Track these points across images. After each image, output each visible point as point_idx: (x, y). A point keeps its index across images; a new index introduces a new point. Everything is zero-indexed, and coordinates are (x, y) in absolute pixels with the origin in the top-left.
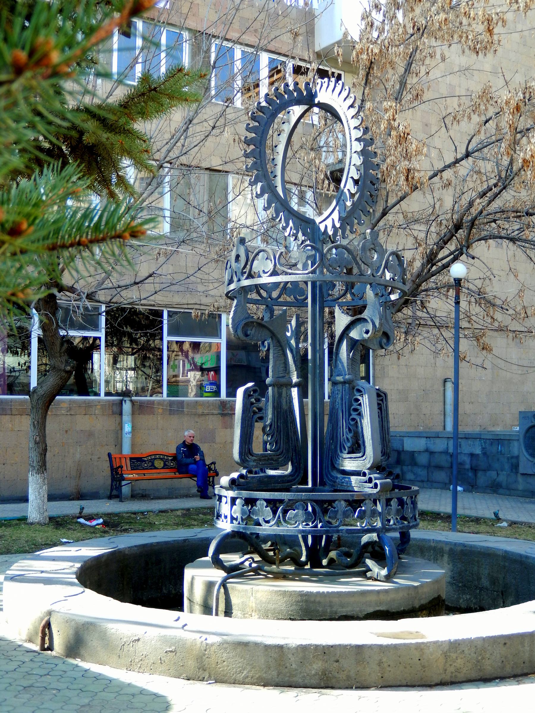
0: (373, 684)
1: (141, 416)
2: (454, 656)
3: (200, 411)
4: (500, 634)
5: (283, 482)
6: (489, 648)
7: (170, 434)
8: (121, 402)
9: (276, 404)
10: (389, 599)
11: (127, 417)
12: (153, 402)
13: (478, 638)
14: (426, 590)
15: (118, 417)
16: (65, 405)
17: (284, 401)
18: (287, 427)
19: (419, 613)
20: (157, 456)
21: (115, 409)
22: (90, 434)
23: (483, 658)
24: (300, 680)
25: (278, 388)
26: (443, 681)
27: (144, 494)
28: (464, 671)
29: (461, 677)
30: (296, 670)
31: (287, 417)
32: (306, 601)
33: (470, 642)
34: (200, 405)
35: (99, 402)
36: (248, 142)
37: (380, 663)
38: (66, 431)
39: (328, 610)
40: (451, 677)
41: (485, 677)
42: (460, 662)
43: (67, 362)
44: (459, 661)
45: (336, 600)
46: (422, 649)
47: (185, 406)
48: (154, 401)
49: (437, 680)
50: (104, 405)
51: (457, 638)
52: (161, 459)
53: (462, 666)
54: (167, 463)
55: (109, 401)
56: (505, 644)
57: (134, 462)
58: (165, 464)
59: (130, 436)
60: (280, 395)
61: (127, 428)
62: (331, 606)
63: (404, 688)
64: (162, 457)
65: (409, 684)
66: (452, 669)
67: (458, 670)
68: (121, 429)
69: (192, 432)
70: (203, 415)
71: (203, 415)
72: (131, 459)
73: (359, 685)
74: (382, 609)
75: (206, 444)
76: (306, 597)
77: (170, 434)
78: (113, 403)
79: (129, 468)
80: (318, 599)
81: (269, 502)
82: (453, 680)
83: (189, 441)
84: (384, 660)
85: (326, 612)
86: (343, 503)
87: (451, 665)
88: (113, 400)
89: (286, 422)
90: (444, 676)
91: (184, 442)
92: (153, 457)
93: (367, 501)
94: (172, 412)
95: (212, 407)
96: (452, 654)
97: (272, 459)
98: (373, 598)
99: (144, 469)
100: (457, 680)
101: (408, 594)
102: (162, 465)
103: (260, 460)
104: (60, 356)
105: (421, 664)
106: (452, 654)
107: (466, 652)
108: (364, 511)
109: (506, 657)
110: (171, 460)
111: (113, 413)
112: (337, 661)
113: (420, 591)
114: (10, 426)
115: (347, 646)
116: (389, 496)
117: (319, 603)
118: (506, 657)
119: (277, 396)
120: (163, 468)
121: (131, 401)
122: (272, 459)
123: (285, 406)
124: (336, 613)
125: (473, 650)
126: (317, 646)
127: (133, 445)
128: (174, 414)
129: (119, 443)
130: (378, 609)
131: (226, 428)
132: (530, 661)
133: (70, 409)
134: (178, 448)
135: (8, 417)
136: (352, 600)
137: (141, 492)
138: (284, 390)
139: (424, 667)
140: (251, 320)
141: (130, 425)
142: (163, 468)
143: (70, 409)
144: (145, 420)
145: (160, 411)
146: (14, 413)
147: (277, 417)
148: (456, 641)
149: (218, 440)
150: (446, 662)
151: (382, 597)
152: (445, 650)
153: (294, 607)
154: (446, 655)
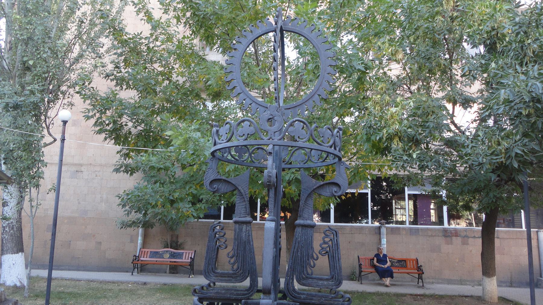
12: (399, 228)
61: (384, 241)
111: (376, 233)
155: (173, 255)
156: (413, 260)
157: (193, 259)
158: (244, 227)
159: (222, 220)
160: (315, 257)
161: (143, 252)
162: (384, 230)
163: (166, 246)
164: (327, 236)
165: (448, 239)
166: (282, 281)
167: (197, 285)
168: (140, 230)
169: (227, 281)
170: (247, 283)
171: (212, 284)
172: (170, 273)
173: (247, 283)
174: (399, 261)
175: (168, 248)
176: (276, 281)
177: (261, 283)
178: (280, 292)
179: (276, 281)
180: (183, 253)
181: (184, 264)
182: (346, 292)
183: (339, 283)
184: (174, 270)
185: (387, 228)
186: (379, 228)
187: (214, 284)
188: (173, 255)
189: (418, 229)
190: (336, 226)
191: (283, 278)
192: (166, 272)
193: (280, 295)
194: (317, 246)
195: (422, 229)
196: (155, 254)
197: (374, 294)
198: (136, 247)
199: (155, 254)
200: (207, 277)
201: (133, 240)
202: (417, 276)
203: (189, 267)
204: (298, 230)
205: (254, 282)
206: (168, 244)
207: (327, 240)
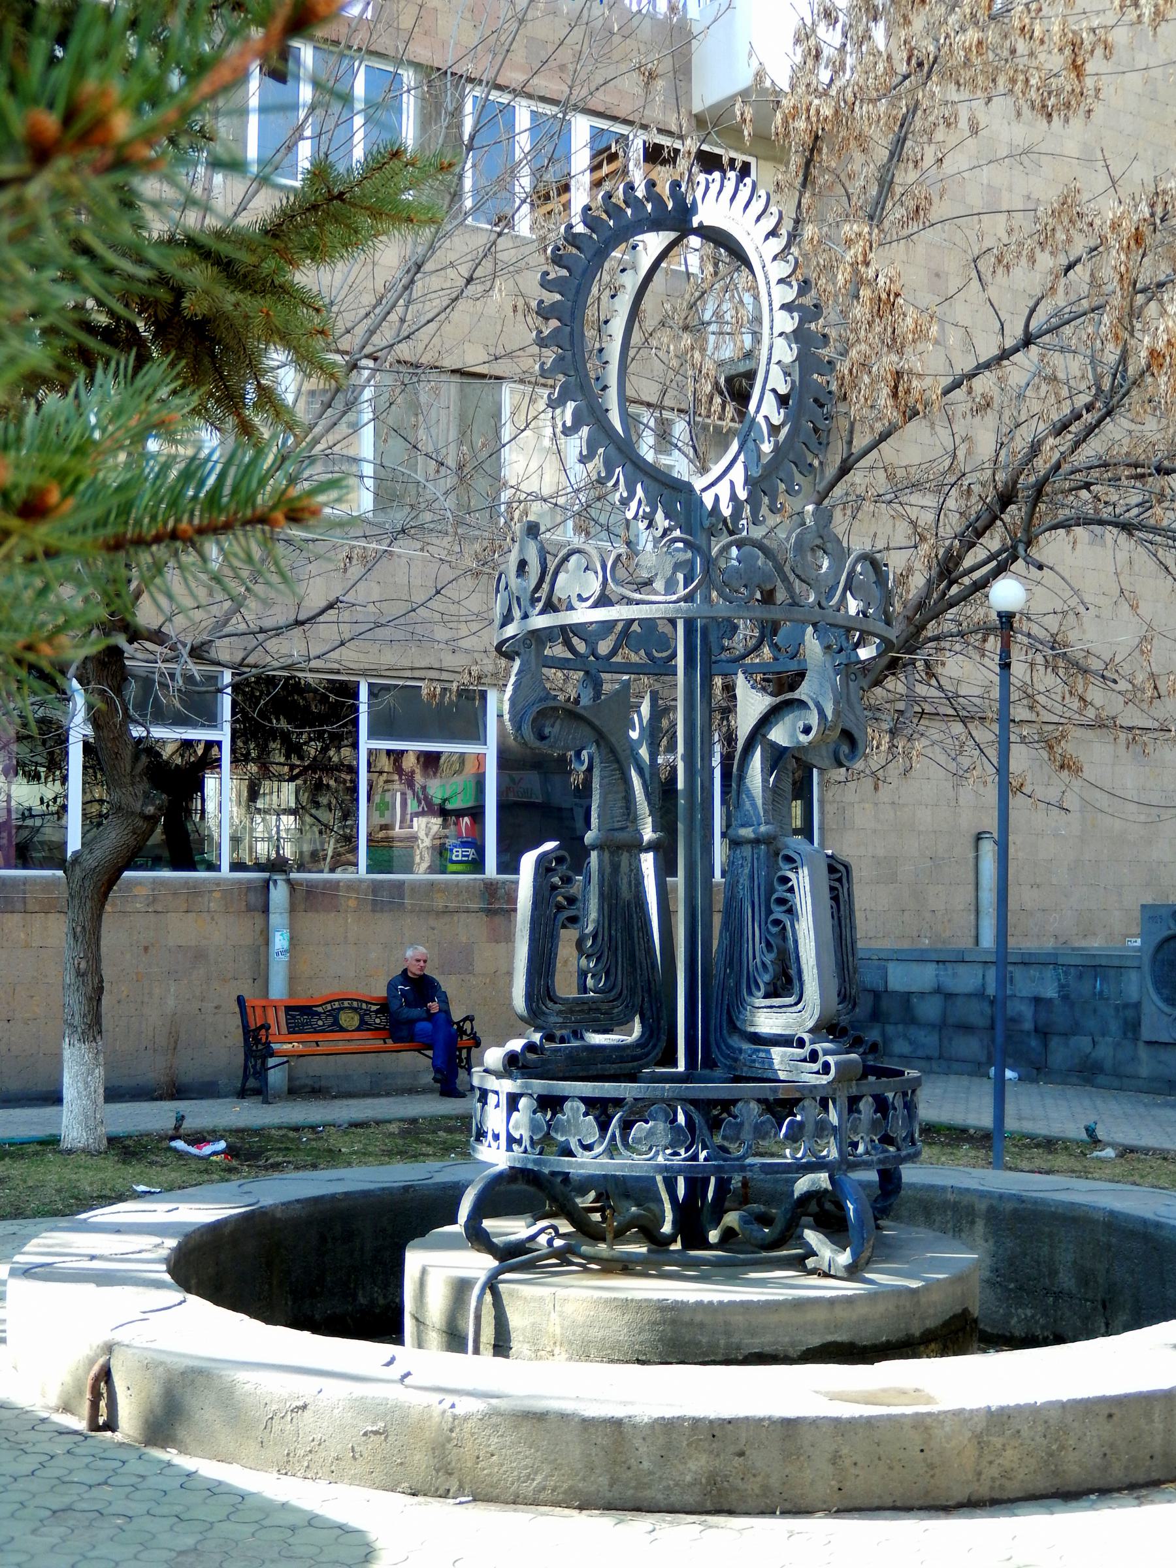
0: (820, 1505)
1: (309, 914)
2: (997, 1442)
3: (440, 903)
4: (1099, 1394)
5: (622, 1060)
6: (1076, 1424)
7: (373, 955)
8: (266, 885)
9: (606, 889)
10: (855, 1317)
11: (278, 918)
12: (336, 885)
13: (1051, 1403)
14: (935, 1297)
15: (259, 918)
16: (143, 891)
17: (625, 881)
18: (631, 938)
19: (922, 1348)
20: (346, 1004)
21: (253, 898)
22: (199, 955)
23: (1062, 1448)
24: (660, 1496)
25: (612, 853)
26: (973, 1498)
27: (317, 1086)
28: (1021, 1476)
29: (1013, 1488)
30: (651, 1473)
31: (631, 916)
32: (673, 1322)
33: (1032, 1412)
34: (439, 891)
35: (218, 885)
36: (544, 312)
37: (835, 1459)
38: (146, 949)
39: (722, 1342)
40: (992, 1488)
41: (1067, 1488)
42: (1010, 1457)
43: (146, 795)
44: (1009, 1453)
45: (738, 1319)
46: (927, 1428)
47: (407, 892)
48: (338, 882)
49: (960, 1495)
50: (229, 891)
51: (1004, 1403)
52: (355, 1010)
53: (1015, 1466)
54: (367, 1018)
55: (239, 882)
56: (1110, 1416)
57: (294, 1017)
58: (362, 1022)
59: (285, 958)
60: (616, 868)
61: (280, 941)
62: (728, 1334)
63: (887, 1513)
64: (355, 1004)
65: (898, 1504)
66: (994, 1471)
67: (1006, 1475)
68: (267, 942)
69: (422, 949)
70: (446, 912)
71: (446, 912)
72: (288, 1009)
73: (788, 1506)
74: (839, 1339)
75: (453, 978)
76: (672, 1313)
77: (373, 955)
78: (249, 887)
79: (284, 1030)
80: (698, 1318)
81: (591, 1103)
82: (996, 1495)
83: (415, 970)
84: (845, 1451)
85: (718, 1346)
86: (754, 1107)
87: (991, 1463)
88: (250, 881)
89: (628, 928)
90: (975, 1486)
91: (405, 971)
92: (337, 1005)
93: (806, 1103)
94: (377, 906)
95: (465, 895)
96: (994, 1439)
97: (598, 1010)
98: (821, 1315)
99: (316, 1032)
100: (1005, 1496)
101: (897, 1307)
102: (356, 1022)
103: (572, 1012)
104: (133, 784)
105: (925, 1460)
106: (994, 1439)
107: (1025, 1432)
108: (801, 1124)
109: (1112, 1446)
110: (377, 1012)
111: (249, 909)
112: (741, 1454)
113: (923, 1300)
114: (22, 936)
115: (762, 1420)
116: (854, 1091)
117: (702, 1325)
118: (1112, 1446)
119: (608, 870)
120: (358, 1029)
121: (288, 881)
122: (598, 1010)
123: (626, 893)
124: (738, 1348)
125: (1040, 1429)
126: (696, 1421)
127: (292, 979)
128: (382, 911)
129: (261, 975)
130: (830, 1338)
131: (497, 942)
132: (1165, 1454)
133: (155, 899)
134: (391, 986)
135: (17, 917)
136: (773, 1319)
137: (309, 1082)
138: (625, 857)
139: (932, 1466)
140: (552, 704)
141: (287, 935)
142: (358, 1029)
143: (155, 899)
144: (319, 924)
145: (352, 903)
146: (30, 908)
147: (610, 912)
148: (1002, 1409)
149: (479, 967)
150: (980, 1456)
151: (841, 1313)
152: (979, 1430)
153: (645, 1336)
154: (980, 1441)
165: (499, 919)
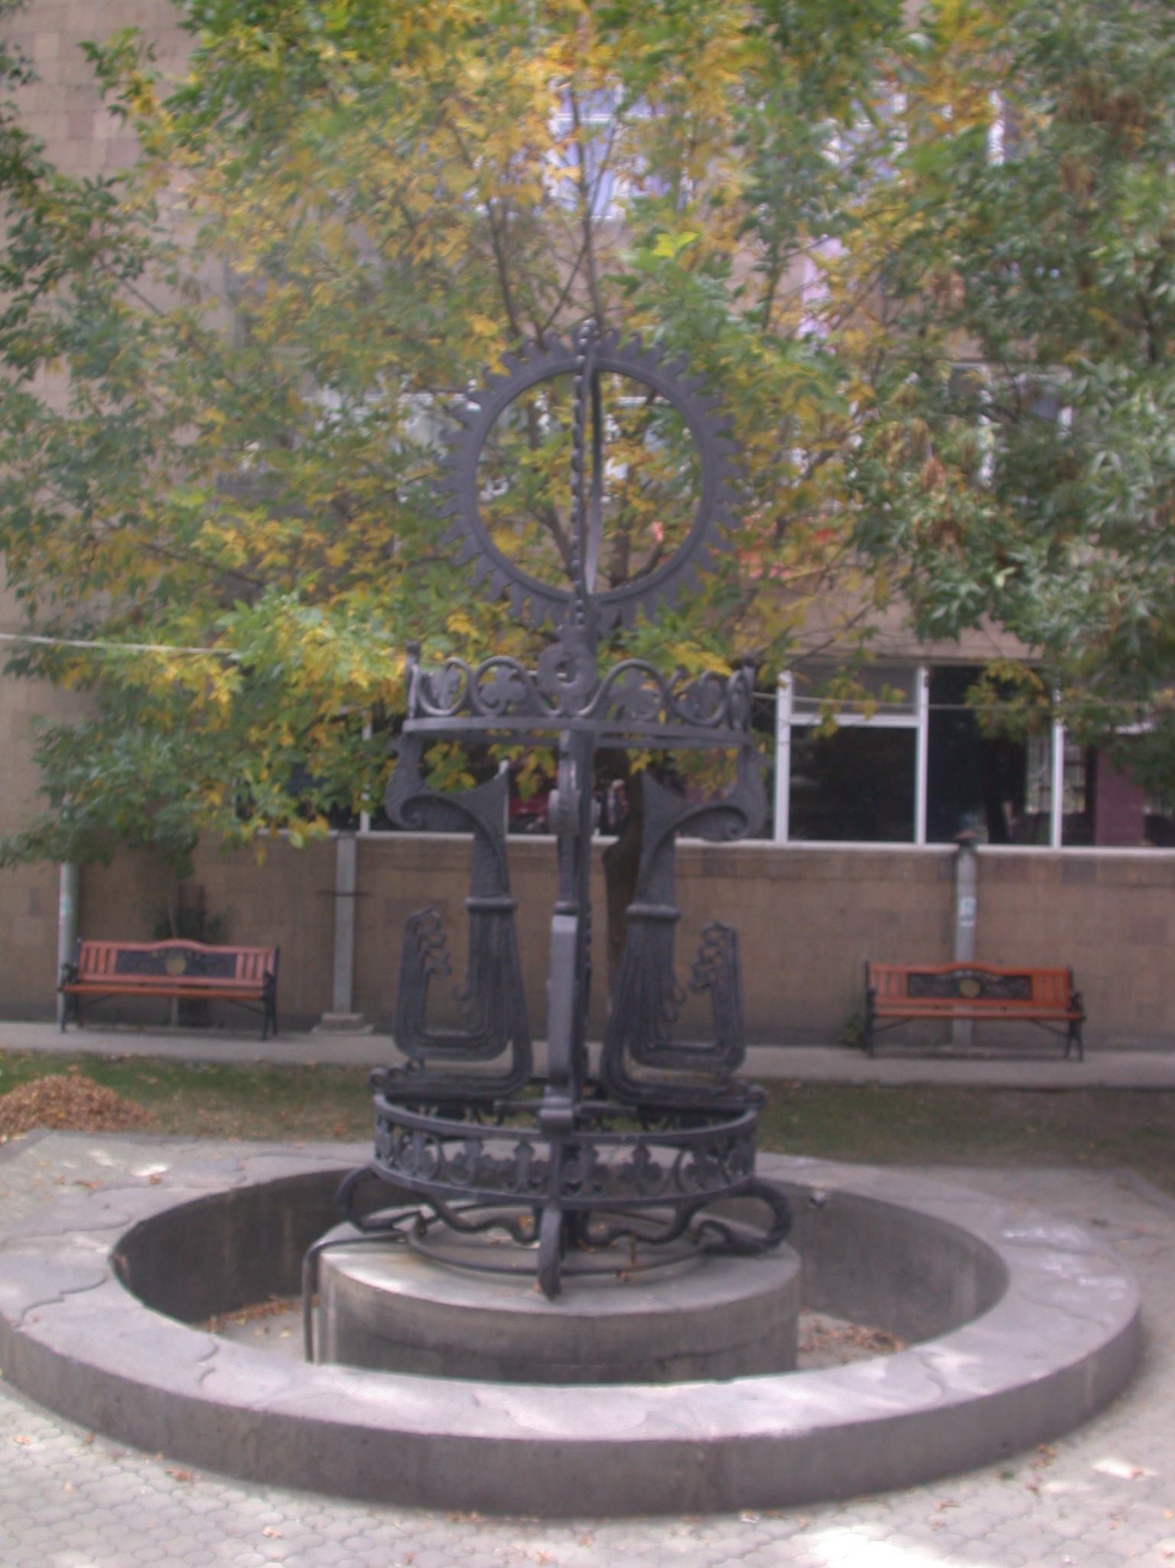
52: (976, 979)
61: (966, 906)
72: (911, 975)
127: (978, 944)
155: (197, 964)
156: (1054, 975)
157: (271, 980)
158: (495, 923)
159: (365, 830)
160: (678, 995)
161: (93, 954)
162: (966, 867)
163: (163, 933)
164: (710, 943)
166: (595, 1050)
167: (378, 1066)
168: (65, 872)
169: (453, 1057)
170: (505, 1060)
171: (416, 1065)
172: (182, 1023)
173: (505, 1060)
174: (1010, 979)
175: (168, 936)
176: (579, 1055)
177: (543, 1055)
178: (589, 1082)
179: (579, 1055)
180: (234, 957)
181: (241, 993)
182: (753, 1080)
183: (737, 1057)
184: (196, 1014)
185: (979, 859)
186: (954, 858)
187: (422, 1062)
188: (197, 964)
189: (1089, 863)
190: (794, 852)
191: (595, 1039)
192: (166, 1022)
193: (588, 1091)
194: (682, 972)
195: (1107, 863)
196: (130, 962)
197: (902, 1087)
198: (54, 930)
199: (130, 962)
200: (402, 1045)
201: (42, 907)
202: (1063, 1026)
203: (261, 1006)
204: (637, 930)
205: (523, 1057)
206: (168, 923)
207: (710, 952)
